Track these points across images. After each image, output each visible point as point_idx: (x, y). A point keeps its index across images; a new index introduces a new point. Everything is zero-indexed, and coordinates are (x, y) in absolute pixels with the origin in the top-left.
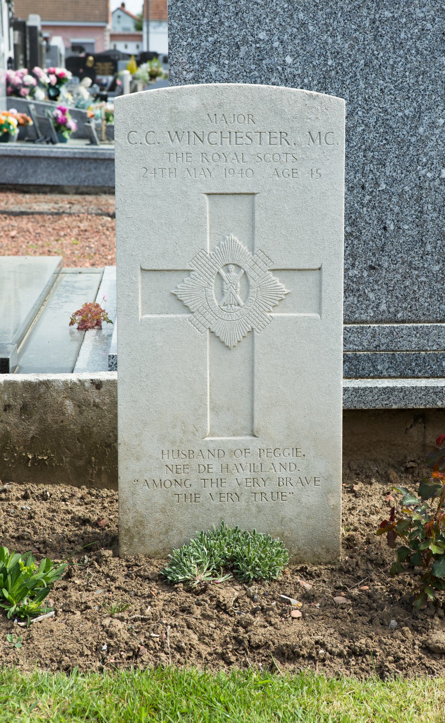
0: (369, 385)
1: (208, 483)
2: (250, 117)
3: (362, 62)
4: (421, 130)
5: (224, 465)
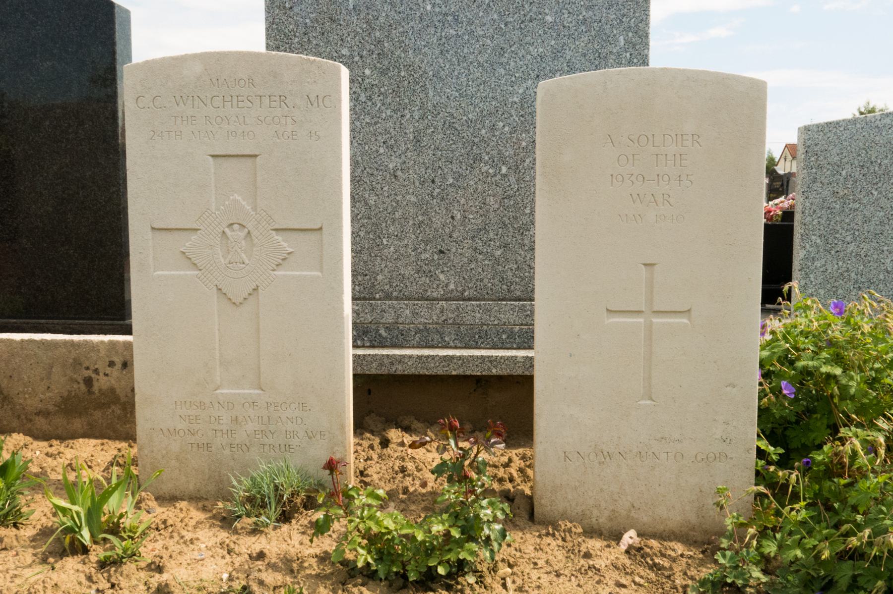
0: (432, 354)
1: (219, 434)
2: (251, 81)
3: (431, 73)
4: (483, 132)
5: (234, 417)
